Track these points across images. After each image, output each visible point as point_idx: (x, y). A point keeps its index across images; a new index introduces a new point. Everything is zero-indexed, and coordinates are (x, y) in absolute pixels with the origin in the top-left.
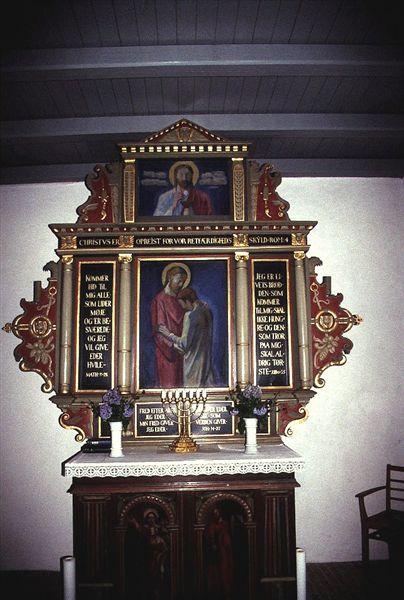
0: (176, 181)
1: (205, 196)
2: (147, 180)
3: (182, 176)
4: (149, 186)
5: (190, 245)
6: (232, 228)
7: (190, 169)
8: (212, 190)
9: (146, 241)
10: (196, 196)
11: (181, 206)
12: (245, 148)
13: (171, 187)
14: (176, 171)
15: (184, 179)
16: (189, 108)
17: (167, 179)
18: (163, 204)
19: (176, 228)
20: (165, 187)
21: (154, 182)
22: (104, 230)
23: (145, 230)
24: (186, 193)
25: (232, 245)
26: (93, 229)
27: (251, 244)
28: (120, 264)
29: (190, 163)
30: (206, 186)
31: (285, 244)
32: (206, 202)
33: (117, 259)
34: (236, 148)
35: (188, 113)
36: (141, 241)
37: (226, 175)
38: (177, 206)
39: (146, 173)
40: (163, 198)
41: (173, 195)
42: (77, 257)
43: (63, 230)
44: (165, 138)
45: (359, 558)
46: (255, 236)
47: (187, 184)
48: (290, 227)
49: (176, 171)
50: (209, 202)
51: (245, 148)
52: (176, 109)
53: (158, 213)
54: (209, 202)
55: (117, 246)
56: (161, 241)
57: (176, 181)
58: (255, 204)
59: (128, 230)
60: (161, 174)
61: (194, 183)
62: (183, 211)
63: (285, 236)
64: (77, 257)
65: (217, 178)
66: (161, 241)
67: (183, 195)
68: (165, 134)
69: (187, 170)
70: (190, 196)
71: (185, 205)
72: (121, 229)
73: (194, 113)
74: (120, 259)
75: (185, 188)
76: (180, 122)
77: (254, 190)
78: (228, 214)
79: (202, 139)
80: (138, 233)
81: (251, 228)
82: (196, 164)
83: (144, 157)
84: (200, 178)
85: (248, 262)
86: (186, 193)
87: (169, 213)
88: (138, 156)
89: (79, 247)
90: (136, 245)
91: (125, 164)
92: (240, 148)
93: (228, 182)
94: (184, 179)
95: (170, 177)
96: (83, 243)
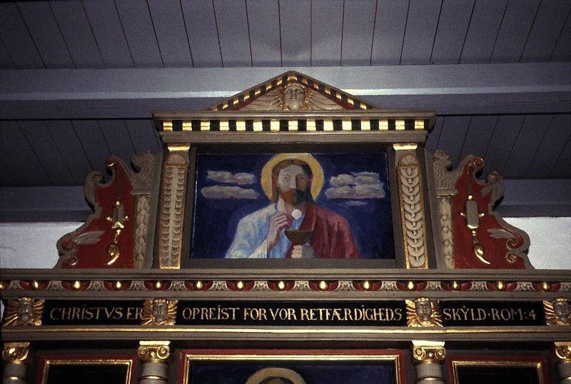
0: (277, 191)
1: (337, 221)
2: (215, 188)
3: (287, 180)
4: (217, 201)
5: (306, 323)
6: (402, 284)
7: (306, 168)
8: (353, 208)
9: (208, 313)
10: (318, 219)
11: (285, 241)
12: (419, 125)
13: (262, 202)
14: (276, 171)
15: (293, 186)
16: (303, 56)
17: (257, 186)
18: (247, 236)
19: (273, 284)
20: (252, 201)
21: (229, 192)
22: (110, 284)
23: (203, 289)
24: (297, 214)
25: (403, 323)
26: (85, 283)
27: (447, 323)
28: (142, 362)
29: (306, 157)
30: (340, 200)
31: (528, 322)
32: (340, 234)
33: (104, 215)
34: (400, 125)
35: (302, 64)
36: (193, 312)
37: (383, 178)
38: (278, 238)
39: (212, 175)
40: (249, 223)
41: (269, 218)
42: (39, 347)
43: (15, 284)
44: (253, 106)
45: (3, 340)
46: (457, 305)
47: (300, 196)
48: (537, 284)
49: (276, 171)
50: (347, 234)
51: (419, 125)
52: (278, 58)
53: (235, 253)
54: (347, 234)
55: (138, 322)
56: (240, 314)
57: (277, 191)
58: (448, 236)
59: (166, 284)
60: (248, 177)
61: (315, 194)
62: (290, 250)
63: (526, 306)
64: (39, 347)
65: (365, 186)
66: (240, 314)
67: (290, 219)
68: (253, 98)
69: (299, 170)
70: (306, 221)
71: (295, 239)
72: (150, 284)
73: (311, 63)
74: (141, 350)
75: (296, 205)
76: (285, 77)
77: (446, 208)
78: (393, 257)
79: (331, 106)
80: (188, 295)
81: (446, 284)
82: (318, 158)
83: (209, 140)
84: (327, 185)
85: (443, 363)
86: (297, 214)
87: (260, 252)
88: (197, 139)
89: (46, 321)
90: (180, 321)
91: (167, 153)
92: (410, 124)
93: (388, 193)
94: (293, 186)
95: (263, 181)
96: (57, 314)
